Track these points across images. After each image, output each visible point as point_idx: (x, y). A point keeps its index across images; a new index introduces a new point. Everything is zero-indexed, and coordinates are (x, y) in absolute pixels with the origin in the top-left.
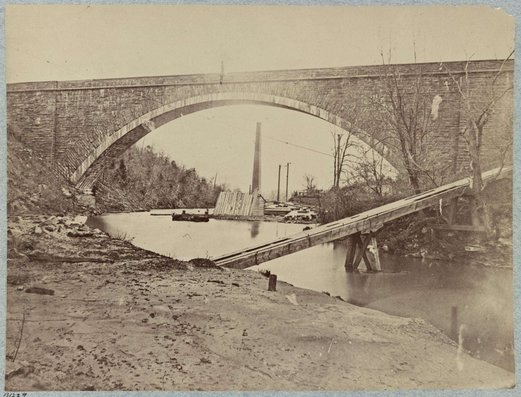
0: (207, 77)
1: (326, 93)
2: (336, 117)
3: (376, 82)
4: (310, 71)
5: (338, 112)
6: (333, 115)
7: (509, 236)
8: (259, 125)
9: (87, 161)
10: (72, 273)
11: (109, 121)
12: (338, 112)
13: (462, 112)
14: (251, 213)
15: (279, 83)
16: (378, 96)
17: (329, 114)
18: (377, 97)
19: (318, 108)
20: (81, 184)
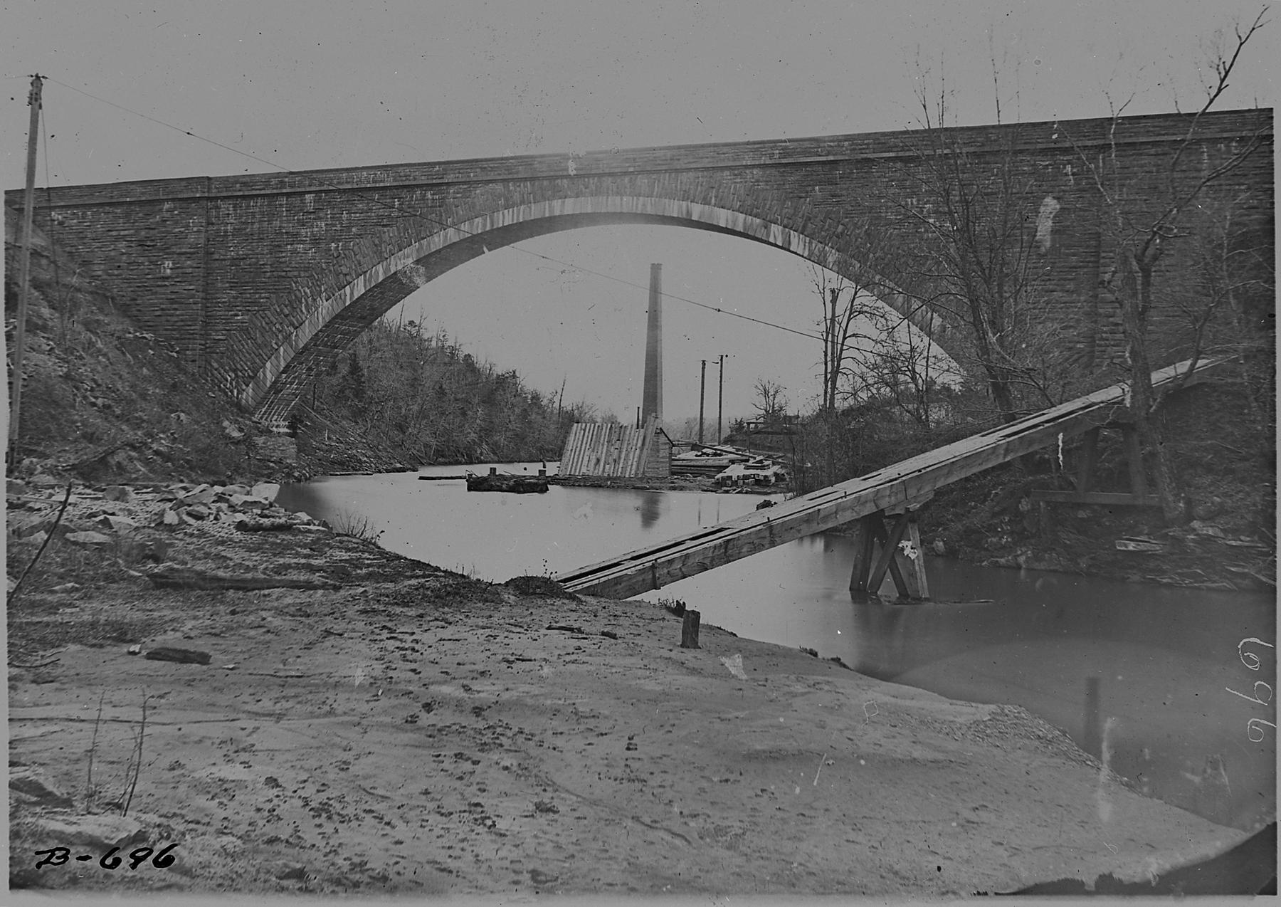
1: (803, 195)
16: (918, 200)
18: (915, 203)
19: (787, 230)
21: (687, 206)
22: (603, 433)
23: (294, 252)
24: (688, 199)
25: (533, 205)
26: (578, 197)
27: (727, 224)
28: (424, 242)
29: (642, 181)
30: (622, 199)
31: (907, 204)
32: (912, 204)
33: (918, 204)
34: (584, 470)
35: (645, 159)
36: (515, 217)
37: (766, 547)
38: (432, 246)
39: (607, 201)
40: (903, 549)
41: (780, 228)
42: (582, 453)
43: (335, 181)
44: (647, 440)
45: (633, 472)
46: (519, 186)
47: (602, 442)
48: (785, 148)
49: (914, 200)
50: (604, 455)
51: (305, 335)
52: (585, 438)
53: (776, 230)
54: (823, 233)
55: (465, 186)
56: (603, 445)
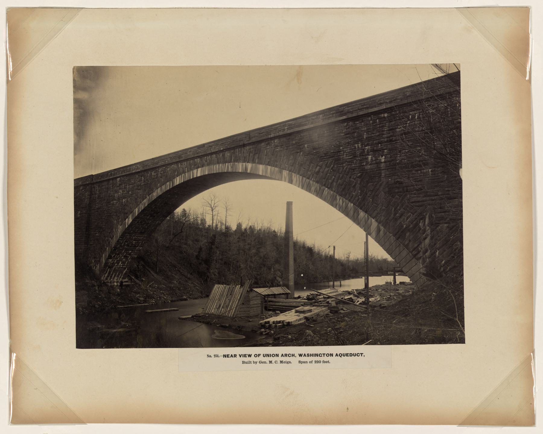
0: (190, 152)
1: (299, 151)
2: (311, 182)
3: (358, 125)
4: (281, 125)
5: (313, 175)
6: (308, 180)
7: (291, 182)
8: (289, 205)
9: (106, 252)
10: (411, 148)
11: (120, 210)
12: (313, 175)
13: (232, 238)
14: (235, 314)
15: (251, 147)
16: (362, 145)
17: (302, 179)
18: (360, 146)
19: (291, 173)
20: (106, 275)
21: (246, 165)
22: (226, 291)
23: (113, 204)
24: (246, 161)
25: (187, 173)
26: (203, 167)
27: (263, 173)
28: (150, 196)
29: (227, 154)
30: (219, 165)
31: (355, 148)
32: (358, 147)
33: (362, 147)
34: (213, 311)
35: (228, 143)
36: (180, 181)
37: (458, 88)
38: (153, 198)
39: (214, 167)
40: (351, 180)
41: (288, 172)
42: (215, 300)
43: (126, 171)
44: (242, 296)
45: (232, 314)
46: (182, 165)
47: (224, 295)
48: (290, 125)
49: (359, 145)
50: (223, 303)
51: (114, 242)
52: (218, 293)
53: (285, 173)
54: (309, 172)
55: (164, 168)
56: (224, 297)
